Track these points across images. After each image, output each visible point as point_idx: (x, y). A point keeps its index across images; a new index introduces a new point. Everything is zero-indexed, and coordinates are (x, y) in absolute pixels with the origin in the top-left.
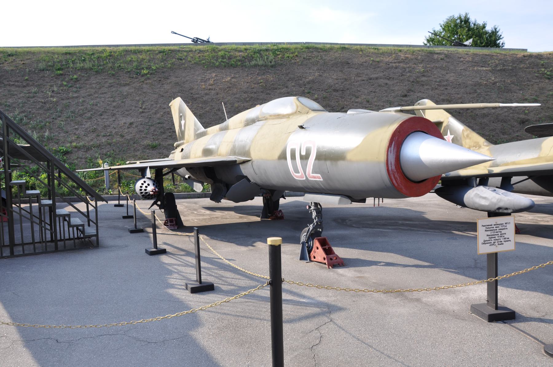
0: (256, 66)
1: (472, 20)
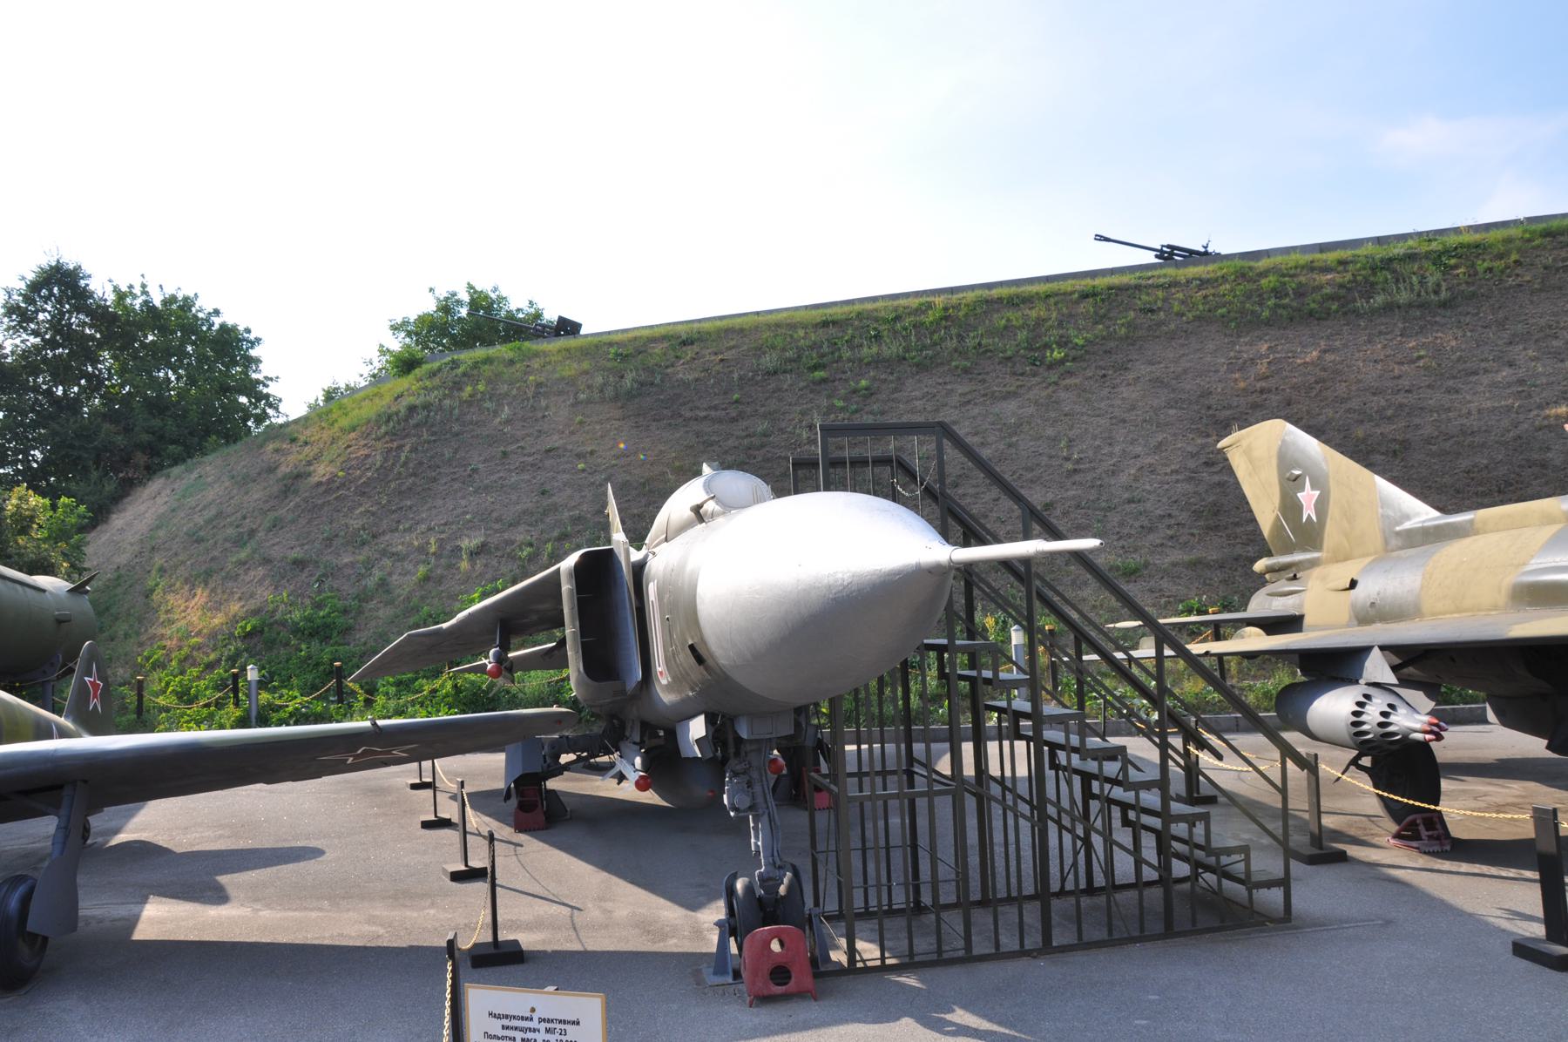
0: (1389, 308)
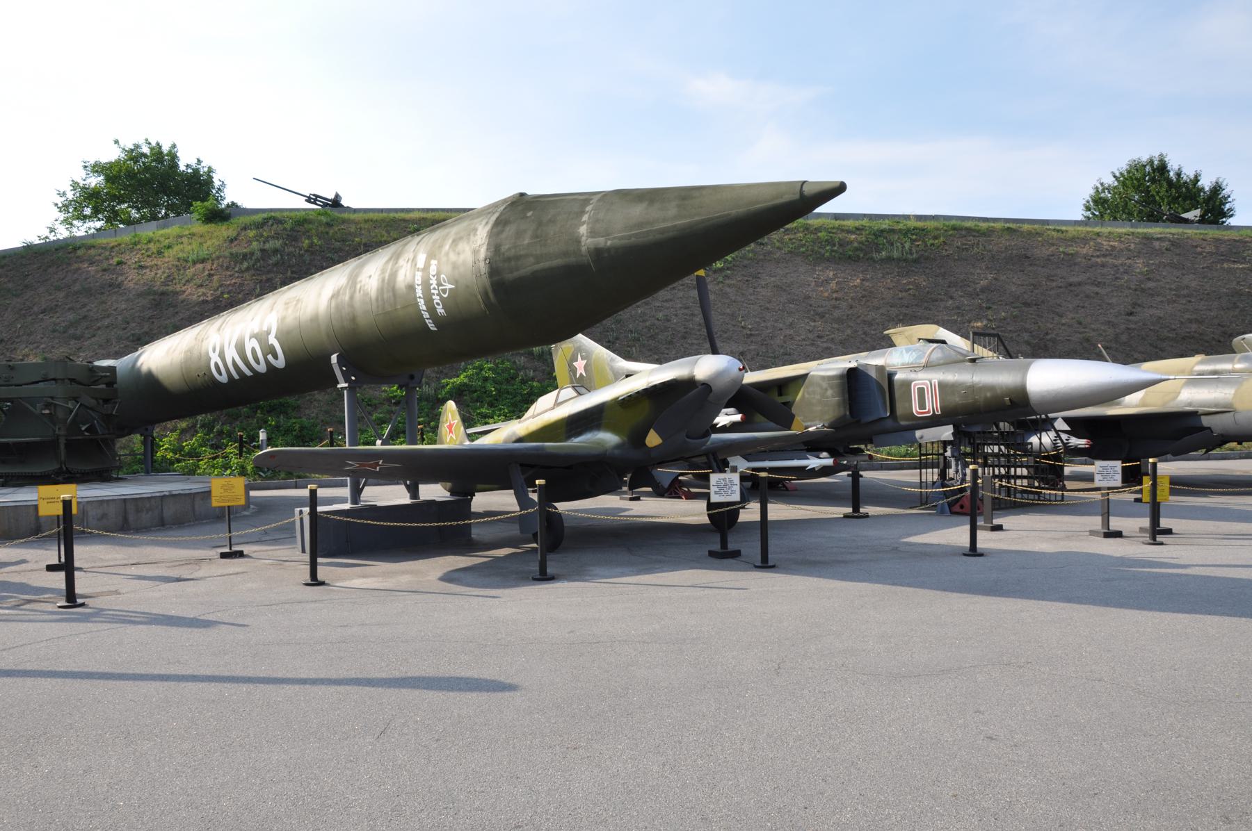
0: (889, 259)
1: (1173, 166)
